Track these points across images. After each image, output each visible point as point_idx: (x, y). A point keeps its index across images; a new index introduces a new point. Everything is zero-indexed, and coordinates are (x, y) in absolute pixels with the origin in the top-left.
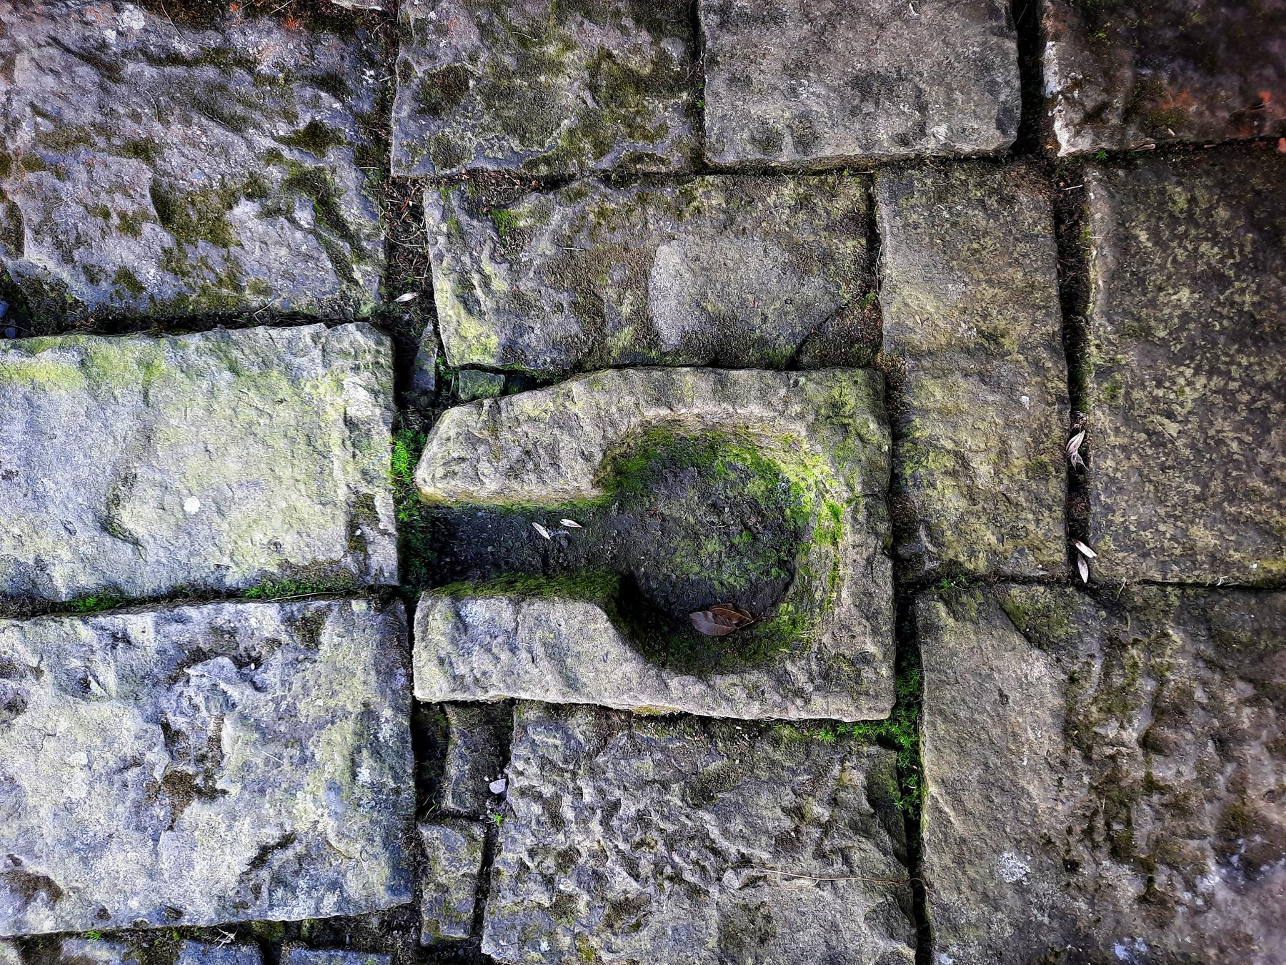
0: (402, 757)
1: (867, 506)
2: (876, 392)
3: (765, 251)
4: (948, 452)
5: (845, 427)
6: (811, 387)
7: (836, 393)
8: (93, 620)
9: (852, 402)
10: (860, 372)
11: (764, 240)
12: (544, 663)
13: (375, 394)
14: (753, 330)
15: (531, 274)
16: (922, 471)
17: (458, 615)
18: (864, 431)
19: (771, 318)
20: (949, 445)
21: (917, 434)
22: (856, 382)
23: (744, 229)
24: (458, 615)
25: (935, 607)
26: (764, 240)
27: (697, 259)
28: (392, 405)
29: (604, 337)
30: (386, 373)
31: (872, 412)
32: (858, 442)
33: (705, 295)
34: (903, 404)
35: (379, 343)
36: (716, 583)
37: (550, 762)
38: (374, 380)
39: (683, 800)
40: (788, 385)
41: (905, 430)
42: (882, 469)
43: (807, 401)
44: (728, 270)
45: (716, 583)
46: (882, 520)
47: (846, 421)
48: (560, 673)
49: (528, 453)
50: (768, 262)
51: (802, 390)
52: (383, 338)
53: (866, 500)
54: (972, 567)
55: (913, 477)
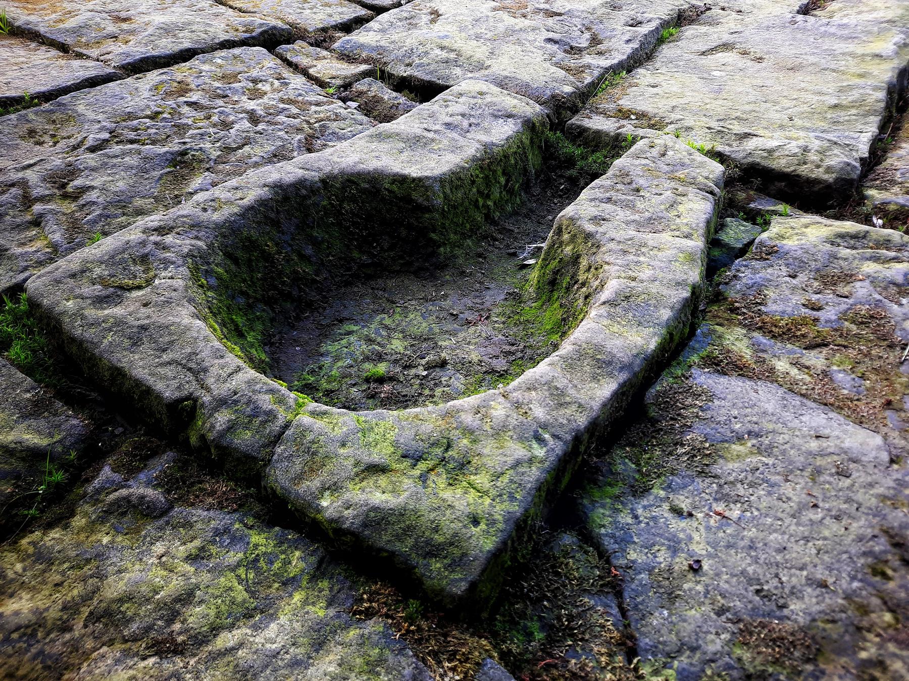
0: (431, 73)
1: (271, 416)
2: (433, 551)
3: (823, 585)
4: (216, 630)
5: (416, 458)
6: (518, 451)
7: (482, 480)
8: (658, 22)
9: (447, 494)
10: (489, 544)
11: (848, 597)
12: (419, 132)
13: (770, 152)
14: (669, 487)
15: (878, 297)
16: (234, 556)
17: (510, 116)
18: (383, 480)
19: (677, 525)
20: (226, 640)
21: (298, 597)
22: (476, 522)
23: (884, 575)
24: (510, 116)
25: (51, 435)
26: (848, 597)
27: (843, 473)
28: (750, 160)
29: (750, 327)
30: (789, 165)
31: (401, 513)
32: (375, 458)
33: (767, 451)
34: (369, 614)
35: (829, 170)
36: (355, 328)
37: (335, 120)
38: (787, 153)
39: (201, 149)
40: (545, 426)
41: (324, 584)
42: (300, 477)
43: (499, 432)
44: (802, 507)
45: (355, 328)
46: (231, 427)
47: (422, 466)
48: (398, 135)
49: (638, 190)
50: (797, 579)
51: (521, 439)
52: (834, 176)
53: (280, 422)
54: (24, 542)
55: (236, 540)
